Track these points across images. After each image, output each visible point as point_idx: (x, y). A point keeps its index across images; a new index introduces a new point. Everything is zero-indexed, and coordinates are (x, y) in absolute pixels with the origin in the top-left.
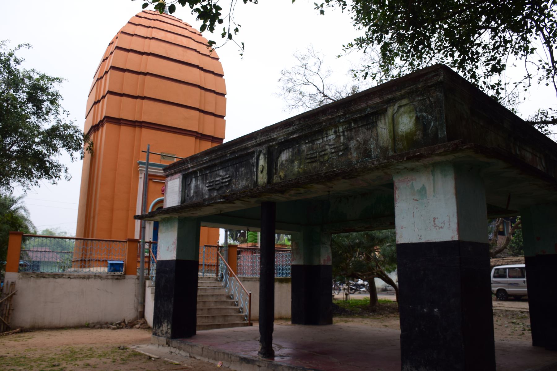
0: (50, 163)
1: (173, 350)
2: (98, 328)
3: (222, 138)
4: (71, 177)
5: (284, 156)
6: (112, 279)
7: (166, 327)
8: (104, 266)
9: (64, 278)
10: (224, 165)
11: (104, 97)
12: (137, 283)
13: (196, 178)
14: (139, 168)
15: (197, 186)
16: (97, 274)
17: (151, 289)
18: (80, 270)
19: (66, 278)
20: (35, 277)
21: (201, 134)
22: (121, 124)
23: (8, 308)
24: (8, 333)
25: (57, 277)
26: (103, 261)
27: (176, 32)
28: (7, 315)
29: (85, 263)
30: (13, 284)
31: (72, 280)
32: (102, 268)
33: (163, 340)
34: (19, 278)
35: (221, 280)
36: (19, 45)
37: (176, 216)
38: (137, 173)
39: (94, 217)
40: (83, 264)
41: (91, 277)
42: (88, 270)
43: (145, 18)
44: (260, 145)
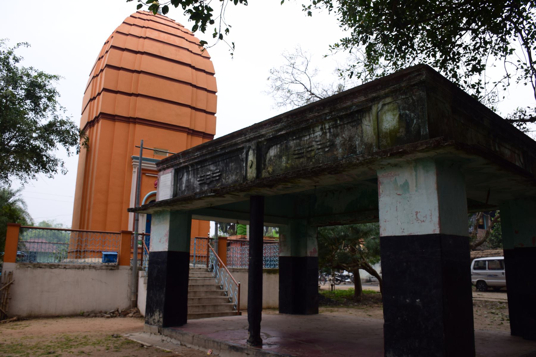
0: (47, 158)
1: (165, 338)
4: (68, 171)
5: (273, 152)
6: (106, 269)
7: (158, 316)
8: (99, 257)
10: (214, 160)
13: (188, 172)
14: (133, 162)
15: (188, 181)
16: (92, 265)
18: (75, 260)
19: (62, 268)
20: (32, 267)
23: (6, 297)
25: (53, 267)
27: (169, 32)
29: (80, 254)
30: (11, 274)
31: (67, 270)
33: (155, 328)
34: (17, 268)
35: (212, 271)
37: (168, 209)
38: (131, 167)
39: (89, 210)
41: (86, 267)
42: (83, 260)
43: (139, 18)
44: (249, 141)
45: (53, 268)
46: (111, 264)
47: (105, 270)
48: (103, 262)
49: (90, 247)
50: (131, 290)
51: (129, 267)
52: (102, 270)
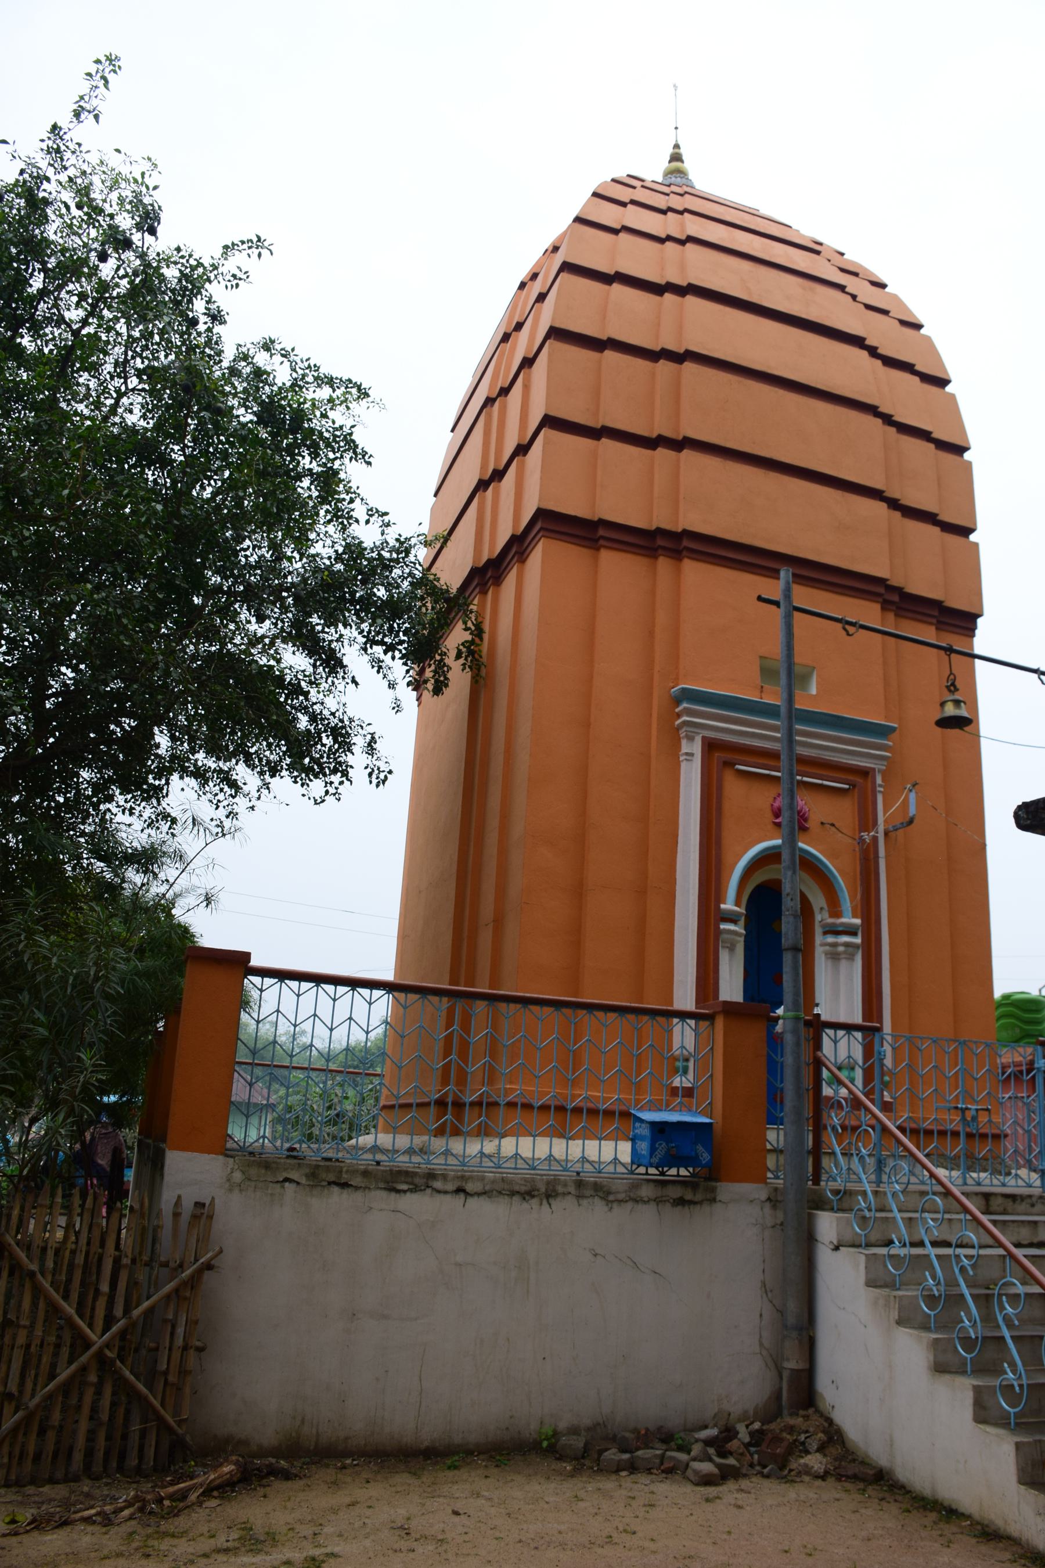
0: (313, 718)
2: (617, 1469)
3: (973, 611)
4: (390, 772)
6: (658, 1201)
8: (616, 1137)
9: (439, 1192)
11: (522, 449)
12: (769, 1221)
14: (679, 716)
17: (863, 1258)
18: (438, 1144)
19: (446, 1192)
20: (303, 1181)
21: (899, 590)
22: (601, 542)
23: (179, 1341)
24: (183, 1496)
25: (405, 1187)
26: (545, 1108)
27: (762, 230)
28: (171, 1378)
29: (459, 1117)
30: (202, 1212)
31: (472, 1202)
32: (539, 1140)
34: (231, 1186)
36: (226, 247)
38: (673, 738)
39: (499, 921)
40: (448, 1116)
41: (560, 1189)
42: (474, 1147)
43: (633, 202)
45: (405, 1192)
46: (673, 1171)
47: (652, 1206)
48: (636, 1158)
49: (518, 1090)
50: (781, 1312)
51: (760, 1192)
52: (640, 1207)
